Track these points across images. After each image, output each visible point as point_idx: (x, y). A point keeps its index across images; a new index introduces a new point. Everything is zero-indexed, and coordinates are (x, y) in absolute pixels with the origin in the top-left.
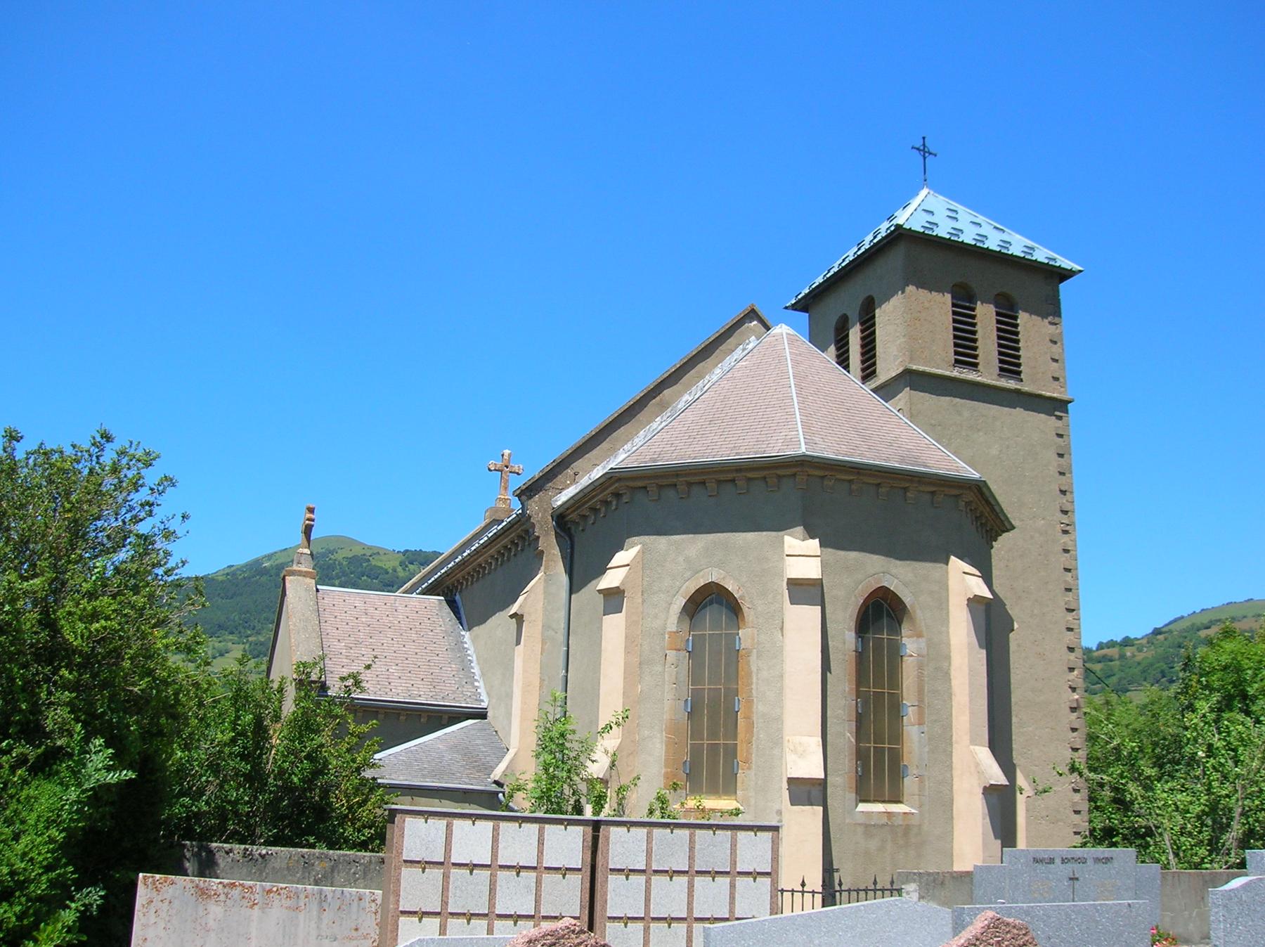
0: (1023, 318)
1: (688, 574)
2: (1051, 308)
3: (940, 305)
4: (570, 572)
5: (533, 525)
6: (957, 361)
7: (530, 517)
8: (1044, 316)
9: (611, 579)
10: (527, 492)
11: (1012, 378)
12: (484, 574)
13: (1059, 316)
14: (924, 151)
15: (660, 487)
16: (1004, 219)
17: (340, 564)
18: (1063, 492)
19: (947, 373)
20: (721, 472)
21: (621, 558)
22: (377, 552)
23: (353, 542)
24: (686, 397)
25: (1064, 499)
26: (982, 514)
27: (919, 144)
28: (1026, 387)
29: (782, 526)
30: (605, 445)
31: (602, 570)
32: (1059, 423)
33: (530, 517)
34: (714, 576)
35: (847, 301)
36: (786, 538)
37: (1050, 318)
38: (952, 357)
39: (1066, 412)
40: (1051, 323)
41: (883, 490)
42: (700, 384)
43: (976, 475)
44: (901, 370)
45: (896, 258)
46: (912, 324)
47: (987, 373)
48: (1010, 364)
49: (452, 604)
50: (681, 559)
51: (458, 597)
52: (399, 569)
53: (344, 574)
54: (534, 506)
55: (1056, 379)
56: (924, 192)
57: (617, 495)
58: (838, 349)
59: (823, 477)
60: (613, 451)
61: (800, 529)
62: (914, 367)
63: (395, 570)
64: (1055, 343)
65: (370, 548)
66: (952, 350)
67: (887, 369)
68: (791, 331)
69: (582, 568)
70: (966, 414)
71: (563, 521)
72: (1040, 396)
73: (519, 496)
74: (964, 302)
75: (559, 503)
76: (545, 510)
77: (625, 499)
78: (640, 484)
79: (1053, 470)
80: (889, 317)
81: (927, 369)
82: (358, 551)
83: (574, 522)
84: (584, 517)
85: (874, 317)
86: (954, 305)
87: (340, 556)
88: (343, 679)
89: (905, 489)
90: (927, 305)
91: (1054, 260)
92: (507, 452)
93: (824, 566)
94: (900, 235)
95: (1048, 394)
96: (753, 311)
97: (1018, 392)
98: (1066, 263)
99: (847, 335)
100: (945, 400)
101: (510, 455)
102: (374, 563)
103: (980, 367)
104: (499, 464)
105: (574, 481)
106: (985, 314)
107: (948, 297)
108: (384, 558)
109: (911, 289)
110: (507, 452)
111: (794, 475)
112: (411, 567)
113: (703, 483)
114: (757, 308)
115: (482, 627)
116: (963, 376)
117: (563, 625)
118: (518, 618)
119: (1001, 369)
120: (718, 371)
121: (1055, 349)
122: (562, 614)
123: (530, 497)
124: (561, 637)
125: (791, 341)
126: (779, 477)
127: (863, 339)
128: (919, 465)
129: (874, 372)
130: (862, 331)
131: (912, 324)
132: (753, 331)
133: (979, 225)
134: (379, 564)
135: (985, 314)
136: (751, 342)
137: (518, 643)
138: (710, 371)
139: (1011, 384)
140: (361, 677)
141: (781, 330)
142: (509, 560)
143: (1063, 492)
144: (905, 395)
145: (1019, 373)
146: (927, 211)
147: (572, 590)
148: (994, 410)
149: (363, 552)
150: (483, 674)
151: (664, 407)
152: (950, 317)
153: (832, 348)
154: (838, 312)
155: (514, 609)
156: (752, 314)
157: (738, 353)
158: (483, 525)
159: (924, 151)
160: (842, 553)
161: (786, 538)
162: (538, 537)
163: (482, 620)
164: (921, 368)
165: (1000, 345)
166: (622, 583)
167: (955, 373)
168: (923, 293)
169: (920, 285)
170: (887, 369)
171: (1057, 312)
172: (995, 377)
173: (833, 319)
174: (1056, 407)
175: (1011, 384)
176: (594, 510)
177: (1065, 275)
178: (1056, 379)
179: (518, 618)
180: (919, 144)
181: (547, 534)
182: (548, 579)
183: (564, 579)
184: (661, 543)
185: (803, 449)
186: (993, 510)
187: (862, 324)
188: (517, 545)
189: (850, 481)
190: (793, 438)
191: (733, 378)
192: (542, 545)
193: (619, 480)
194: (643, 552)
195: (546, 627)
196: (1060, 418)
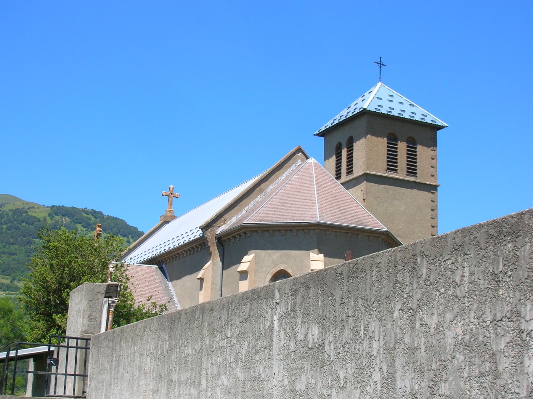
0: (420, 148)
1: (273, 266)
2: (432, 143)
3: (382, 143)
4: (223, 261)
5: (208, 242)
6: (388, 169)
7: (206, 238)
8: (429, 147)
9: (243, 267)
10: (206, 228)
11: (412, 176)
12: (180, 258)
13: (436, 146)
14: (380, 64)
15: (263, 231)
16: (416, 98)
17: (7, 214)
18: (433, 227)
19: (383, 175)
20: (286, 227)
21: (246, 258)
22: (32, 207)
23: (16, 199)
24: (271, 187)
25: (433, 230)
26: (389, 243)
27: (378, 61)
28: (418, 180)
29: (309, 248)
30: (237, 208)
31: (239, 262)
32: (433, 196)
33: (206, 238)
34: (283, 267)
35: (341, 136)
36: (311, 253)
37: (432, 148)
38: (386, 167)
39: (437, 191)
40: (432, 150)
41: (349, 235)
42: (277, 181)
43: (385, 229)
44: (363, 173)
45: (363, 122)
46: (368, 153)
47: (401, 175)
48: (412, 170)
49: (161, 269)
50: (270, 260)
51: (164, 266)
52: (48, 218)
53: (10, 221)
54: (208, 234)
55: (433, 176)
56: (379, 84)
57: (245, 233)
58: (337, 157)
59: (326, 230)
60: (240, 210)
61: (316, 250)
62: (369, 172)
63: (45, 219)
64: (433, 159)
65: (28, 203)
66: (386, 163)
67: (358, 172)
68: (316, 162)
69: (230, 260)
70: (391, 192)
71: (221, 240)
72: (425, 184)
73: (202, 229)
74: (393, 140)
75: (218, 232)
76: (213, 235)
77: (249, 235)
78: (255, 230)
79: (429, 217)
80: (359, 146)
81: (374, 173)
82: (19, 205)
83: (224, 240)
84: (229, 239)
85: (353, 146)
86: (388, 143)
87: (6, 208)
88: (160, 306)
89: (358, 235)
90: (376, 143)
91: (435, 122)
92: (172, 186)
93: (325, 265)
94: (364, 112)
95: (428, 183)
96: (299, 150)
97: (415, 182)
98: (440, 122)
99: (341, 152)
100: (382, 186)
101: (173, 188)
102: (30, 214)
103: (398, 171)
104: (168, 192)
105: (224, 223)
106: (402, 147)
107: (385, 139)
108: (37, 210)
109: (369, 136)
110: (172, 186)
111: (315, 229)
112: (56, 217)
113: (280, 230)
114: (302, 147)
115: (179, 281)
116: (390, 176)
117: (219, 283)
118: (201, 280)
119: (408, 172)
120: (284, 176)
121: (433, 162)
122: (219, 278)
123: (207, 230)
124: (219, 288)
125: (316, 165)
126: (309, 230)
127: (348, 155)
128: (363, 225)
129: (352, 171)
130: (348, 152)
131: (368, 153)
132: (299, 158)
133: (402, 103)
134: (34, 215)
135: (402, 147)
136: (299, 160)
137: (201, 289)
138: (281, 175)
139: (411, 179)
140: (166, 305)
141: (312, 160)
142: (193, 253)
143: (433, 227)
144: (364, 185)
145: (416, 173)
146: (379, 98)
147: (224, 269)
148: (404, 190)
149: (22, 206)
150: (179, 301)
151: (261, 191)
152: (386, 149)
153: (334, 157)
154: (339, 140)
155: (200, 274)
156: (299, 150)
157: (293, 167)
158: (160, 223)
159: (380, 64)
160: (332, 259)
161: (311, 253)
162: (210, 247)
163: (179, 277)
164: (372, 173)
165: (408, 161)
166: (248, 269)
167: (387, 174)
168: (374, 138)
169: (373, 134)
170: (358, 172)
171: (435, 145)
172: (405, 175)
173: (335, 144)
174: (432, 188)
175: (411, 179)
176: (234, 237)
177: (440, 128)
178: (433, 176)
179: (201, 280)
180: (378, 61)
181: (214, 245)
182: (214, 264)
183: (220, 264)
184: (262, 253)
185: (318, 220)
186: (394, 240)
187: (348, 148)
188: (198, 248)
189: (336, 232)
190: (315, 215)
191: (292, 184)
192: (211, 250)
193: (246, 228)
194: (255, 256)
195: (213, 283)
196: (433, 193)
